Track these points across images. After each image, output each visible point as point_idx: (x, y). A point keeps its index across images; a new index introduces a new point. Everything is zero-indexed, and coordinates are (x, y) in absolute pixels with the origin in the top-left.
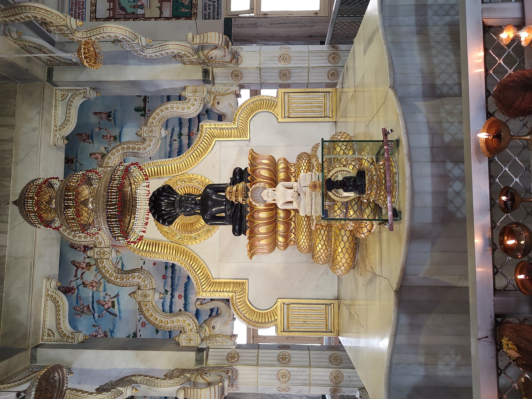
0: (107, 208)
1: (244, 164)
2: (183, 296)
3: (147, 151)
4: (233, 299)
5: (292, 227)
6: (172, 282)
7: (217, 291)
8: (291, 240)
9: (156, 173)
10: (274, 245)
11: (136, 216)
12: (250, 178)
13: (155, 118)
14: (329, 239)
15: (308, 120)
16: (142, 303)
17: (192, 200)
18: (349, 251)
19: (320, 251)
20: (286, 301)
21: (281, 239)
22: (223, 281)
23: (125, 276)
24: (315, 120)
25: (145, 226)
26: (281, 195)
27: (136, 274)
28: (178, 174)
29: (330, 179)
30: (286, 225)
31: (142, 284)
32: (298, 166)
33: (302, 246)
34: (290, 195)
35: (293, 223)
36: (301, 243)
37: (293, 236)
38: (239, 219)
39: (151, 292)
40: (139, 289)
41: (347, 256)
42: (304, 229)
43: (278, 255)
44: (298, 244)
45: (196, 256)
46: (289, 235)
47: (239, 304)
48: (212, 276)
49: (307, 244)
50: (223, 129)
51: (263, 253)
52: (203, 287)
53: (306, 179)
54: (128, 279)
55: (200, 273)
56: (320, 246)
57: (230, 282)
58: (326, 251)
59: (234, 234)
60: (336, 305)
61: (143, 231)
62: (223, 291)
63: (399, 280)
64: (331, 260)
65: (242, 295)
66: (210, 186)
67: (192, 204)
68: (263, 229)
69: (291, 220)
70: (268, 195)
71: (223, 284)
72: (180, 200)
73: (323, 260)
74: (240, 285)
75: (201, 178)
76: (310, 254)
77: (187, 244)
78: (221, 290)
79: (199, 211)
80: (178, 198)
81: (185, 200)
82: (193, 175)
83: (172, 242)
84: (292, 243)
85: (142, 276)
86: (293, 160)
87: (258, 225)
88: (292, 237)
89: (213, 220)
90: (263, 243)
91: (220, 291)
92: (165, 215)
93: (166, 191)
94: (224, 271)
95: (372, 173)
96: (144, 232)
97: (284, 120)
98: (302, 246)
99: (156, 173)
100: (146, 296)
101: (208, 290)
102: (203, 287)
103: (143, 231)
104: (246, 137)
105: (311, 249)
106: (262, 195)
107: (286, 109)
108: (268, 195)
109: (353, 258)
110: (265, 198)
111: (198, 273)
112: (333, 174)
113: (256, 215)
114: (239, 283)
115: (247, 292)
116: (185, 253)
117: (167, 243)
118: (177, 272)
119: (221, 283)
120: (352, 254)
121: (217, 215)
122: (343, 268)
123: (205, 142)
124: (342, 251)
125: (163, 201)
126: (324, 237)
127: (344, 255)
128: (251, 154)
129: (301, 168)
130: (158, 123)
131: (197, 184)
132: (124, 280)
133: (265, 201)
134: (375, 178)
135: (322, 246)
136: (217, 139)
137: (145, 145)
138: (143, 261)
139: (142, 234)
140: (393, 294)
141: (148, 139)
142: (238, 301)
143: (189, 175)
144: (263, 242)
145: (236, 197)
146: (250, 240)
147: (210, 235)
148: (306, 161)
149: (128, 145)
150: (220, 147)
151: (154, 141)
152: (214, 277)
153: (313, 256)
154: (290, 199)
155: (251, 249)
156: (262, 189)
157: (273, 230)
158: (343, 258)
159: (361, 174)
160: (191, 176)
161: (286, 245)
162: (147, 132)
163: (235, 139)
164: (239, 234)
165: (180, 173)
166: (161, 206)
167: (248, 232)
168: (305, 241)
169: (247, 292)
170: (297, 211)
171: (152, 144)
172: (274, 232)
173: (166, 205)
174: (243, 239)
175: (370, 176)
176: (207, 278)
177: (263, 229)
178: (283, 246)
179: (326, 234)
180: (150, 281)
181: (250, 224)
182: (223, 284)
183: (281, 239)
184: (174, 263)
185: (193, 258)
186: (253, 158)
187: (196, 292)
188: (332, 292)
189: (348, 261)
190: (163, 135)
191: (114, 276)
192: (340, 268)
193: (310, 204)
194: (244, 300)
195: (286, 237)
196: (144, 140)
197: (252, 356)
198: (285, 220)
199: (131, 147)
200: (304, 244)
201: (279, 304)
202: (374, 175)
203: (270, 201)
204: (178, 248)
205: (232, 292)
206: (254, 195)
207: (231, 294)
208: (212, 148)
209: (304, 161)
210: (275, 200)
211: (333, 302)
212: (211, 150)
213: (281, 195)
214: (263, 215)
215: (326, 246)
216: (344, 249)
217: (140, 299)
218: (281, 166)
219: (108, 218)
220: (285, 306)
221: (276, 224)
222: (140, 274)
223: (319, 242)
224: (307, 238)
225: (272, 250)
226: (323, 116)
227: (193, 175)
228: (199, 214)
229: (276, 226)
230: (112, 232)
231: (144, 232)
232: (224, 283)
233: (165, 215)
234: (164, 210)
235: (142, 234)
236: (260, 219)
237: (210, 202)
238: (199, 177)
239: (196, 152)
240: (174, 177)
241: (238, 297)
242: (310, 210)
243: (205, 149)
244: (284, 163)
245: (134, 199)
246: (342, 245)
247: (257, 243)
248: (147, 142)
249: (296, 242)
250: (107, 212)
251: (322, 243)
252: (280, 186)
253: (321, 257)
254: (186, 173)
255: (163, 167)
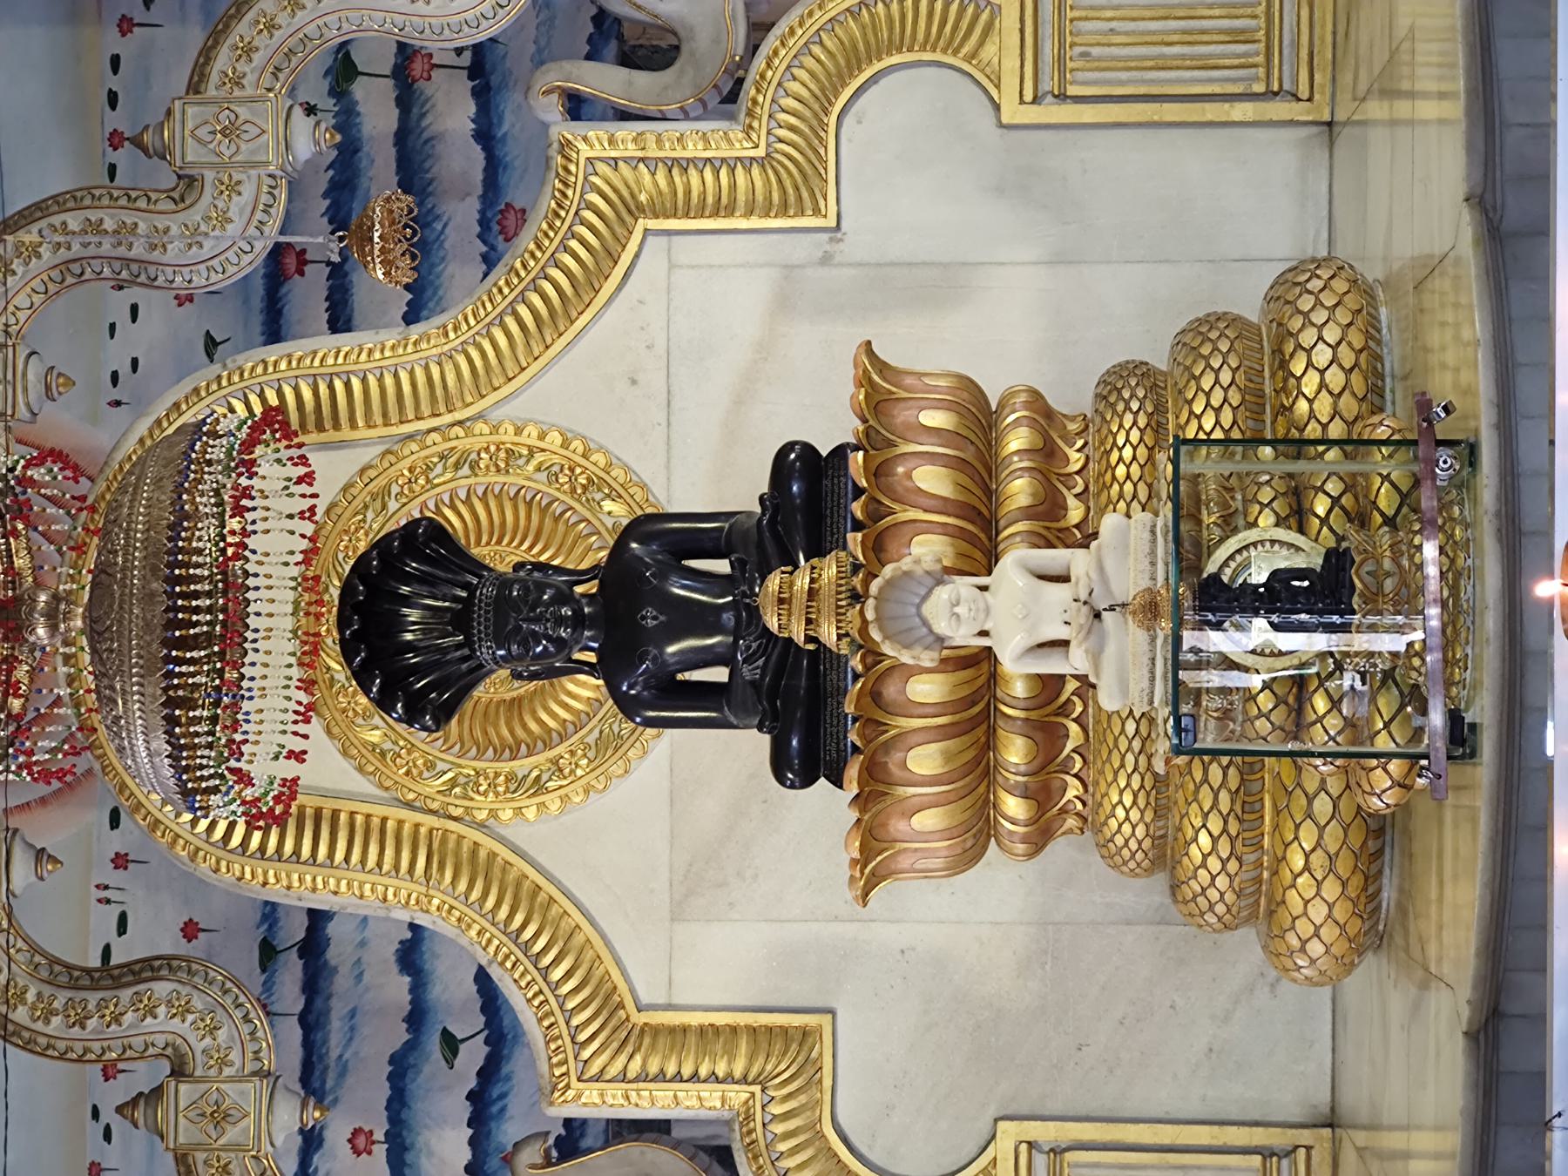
0: (168, 659)
1: (830, 429)
2: (379, 1135)
3: (206, 252)
4: (749, 1117)
5: (1070, 746)
6: (308, 1044)
7: (661, 1077)
8: (1063, 811)
9: (311, 419)
10: (976, 834)
11: (246, 671)
12: (865, 507)
13: (249, 51)
14: (1247, 807)
15: (1172, 112)
16: (201, 1156)
17: (554, 601)
18: (1343, 866)
19: (1204, 865)
20: (1045, 1132)
21: (1014, 806)
22: (695, 1019)
23: (93, 998)
24: (1212, 111)
25: (302, 728)
26: (1015, 612)
27: (162, 988)
28: (435, 422)
29: (1216, 577)
30: (1038, 736)
31: (199, 1047)
32: (1096, 426)
33: (1119, 840)
34: (1054, 611)
35: (1074, 728)
36: (1113, 823)
37: (1074, 789)
38: (809, 717)
39: (246, 1095)
40: (179, 1071)
41: (1331, 890)
42: (1130, 758)
43: (1002, 878)
44: (1098, 829)
45: (541, 881)
46: (1056, 784)
47: (783, 1147)
48: (632, 991)
49: (1140, 831)
50: (684, 165)
51: (926, 873)
52: (586, 1054)
53: (1127, 546)
54: (117, 1019)
55: (568, 974)
56: (1204, 840)
57: (734, 1030)
58: (1233, 866)
59: (780, 779)
60: (1321, 1157)
61: (291, 755)
62: (695, 1077)
63: (1475, 988)
64: (1260, 904)
65: (802, 1099)
66: (644, 526)
67: (560, 621)
68: (925, 760)
69: (1064, 711)
70: (953, 611)
71: (692, 1039)
72: (502, 603)
73: (1220, 909)
74: (789, 1045)
75: (565, 444)
76: (1161, 880)
77: (493, 813)
78: (687, 1071)
79: (591, 657)
80: (489, 591)
81: (523, 598)
82: (519, 431)
83: (409, 805)
84: (1071, 822)
85: (198, 1002)
86: (1072, 396)
87: (903, 740)
88: (1071, 794)
89: (660, 698)
90: (926, 823)
91: (678, 1078)
92: (418, 670)
93: (421, 550)
94: (697, 967)
95: (1379, 563)
96: (299, 756)
97: (1032, 114)
98: (1119, 840)
99: (311, 419)
100: (220, 1117)
101: (613, 1071)
102: (586, 1054)
103: (291, 755)
104: (817, 211)
105: (1164, 854)
106: (927, 610)
107: (1049, 50)
108: (953, 611)
109: (1367, 902)
110: (942, 627)
111: (557, 974)
112: (1231, 557)
113: (890, 690)
114: (784, 1030)
115: (827, 1083)
116: (480, 868)
117: (378, 811)
118: (341, 982)
119: (685, 1029)
120: (1356, 882)
121: (679, 677)
122: (1316, 948)
123: (583, 242)
124: (1307, 868)
125: (407, 601)
126: (1224, 797)
127: (1319, 884)
128: (864, 381)
129: (1115, 456)
130: (267, 80)
131: (540, 483)
132: (92, 1023)
133: (940, 639)
134: (1389, 584)
135: (1215, 840)
136: (653, 224)
137: (195, 216)
138: (115, 911)
139: (289, 769)
140: (1460, 1041)
141: (209, 175)
142: (779, 1128)
143: (495, 430)
144: (927, 820)
145: (809, 621)
146: (863, 811)
147: (617, 769)
148: (1142, 421)
149: (94, 216)
150: (672, 266)
151: (248, 191)
152: (645, 999)
153: (1175, 888)
154: (1061, 633)
155: (868, 850)
156: (929, 581)
157: (977, 761)
158: (1316, 903)
159: (1338, 560)
160: (507, 436)
161: (1040, 835)
162: (202, 133)
163: (755, 222)
164: (807, 781)
165: (447, 419)
166: (401, 625)
167: (852, 772)
168: (1135, 815)
169: (827, 1083)
170: (1087, 686)
171: (238, 206)
172: (977, 773)
173: (421, 626)
174: (827, 804)
175: (1368, 579)
176: (608, 1002)
177: (925, 760)
178: (1025, 840)
179: (1234, 781)
180: (246, 1029)
181: (861, 735)
182: (692, 1039)
183: (1014, 806)
184: (422, 920)
185: (525, 896)
186: (879, 389)
187: (545, 1082)
188: (1296, 1087)
189: (1340, 913)
190: (304, 148)
191: (30, 997)
192: (1303, 950)
193: (1146, 660)
194: (814, 1128)
195: (1041, 794)
196: (189, 182)
197: (1280, 79)
198: (1034, 715)
199: (109, 225)
200: (1127, 828)
201: (1004, 1146)
202: (1388, 574)
203: (963, 637)
204: (444, 841)
205: (744, 1080)
206: (891, 609)
207: (738, 1095)
208: (627, 275)
209: (1128, 420)
210: (984, 633)
211: (1305, 1136)
212: (619, 288)
213: (1015, 612)
214: (927, 689)
215: (1232, 840)
216: (1318, 859)
217: (186, 1133)
218: (1017, 441)
219: (171, 703)
220: (1040, 1161)
221: (991, 732)
222: (184, 990)
223: (1198, 822)
224: (1141, 802)
225: (968, 857)
226: (1259, 88)
227: (519, 431)
228: (590, 669)
229: (989, 744)
230: (187, 769)
231: (299, 756)
232: (702, 1030)
233: (418, 670)
234: (410, 647)
235: (289, 769)
236: (912, 709)
237: (650, 611)
238: (555, 438)
239: (535, 299)
240: (410, 437)
241: (777, 1110)
242: (1145, 684)
243: (588, 283)
244: (1032, 423)
245: (232, 588)
246: (1308, 838)
247: (898, 826)
248: (207, 198)
249: (1090, 822)
250: (170, 675)
251: (1215, 825)
252: (1016, 560)
253: (1213, 894)
254: (480, 417)
255: (348, 385)
